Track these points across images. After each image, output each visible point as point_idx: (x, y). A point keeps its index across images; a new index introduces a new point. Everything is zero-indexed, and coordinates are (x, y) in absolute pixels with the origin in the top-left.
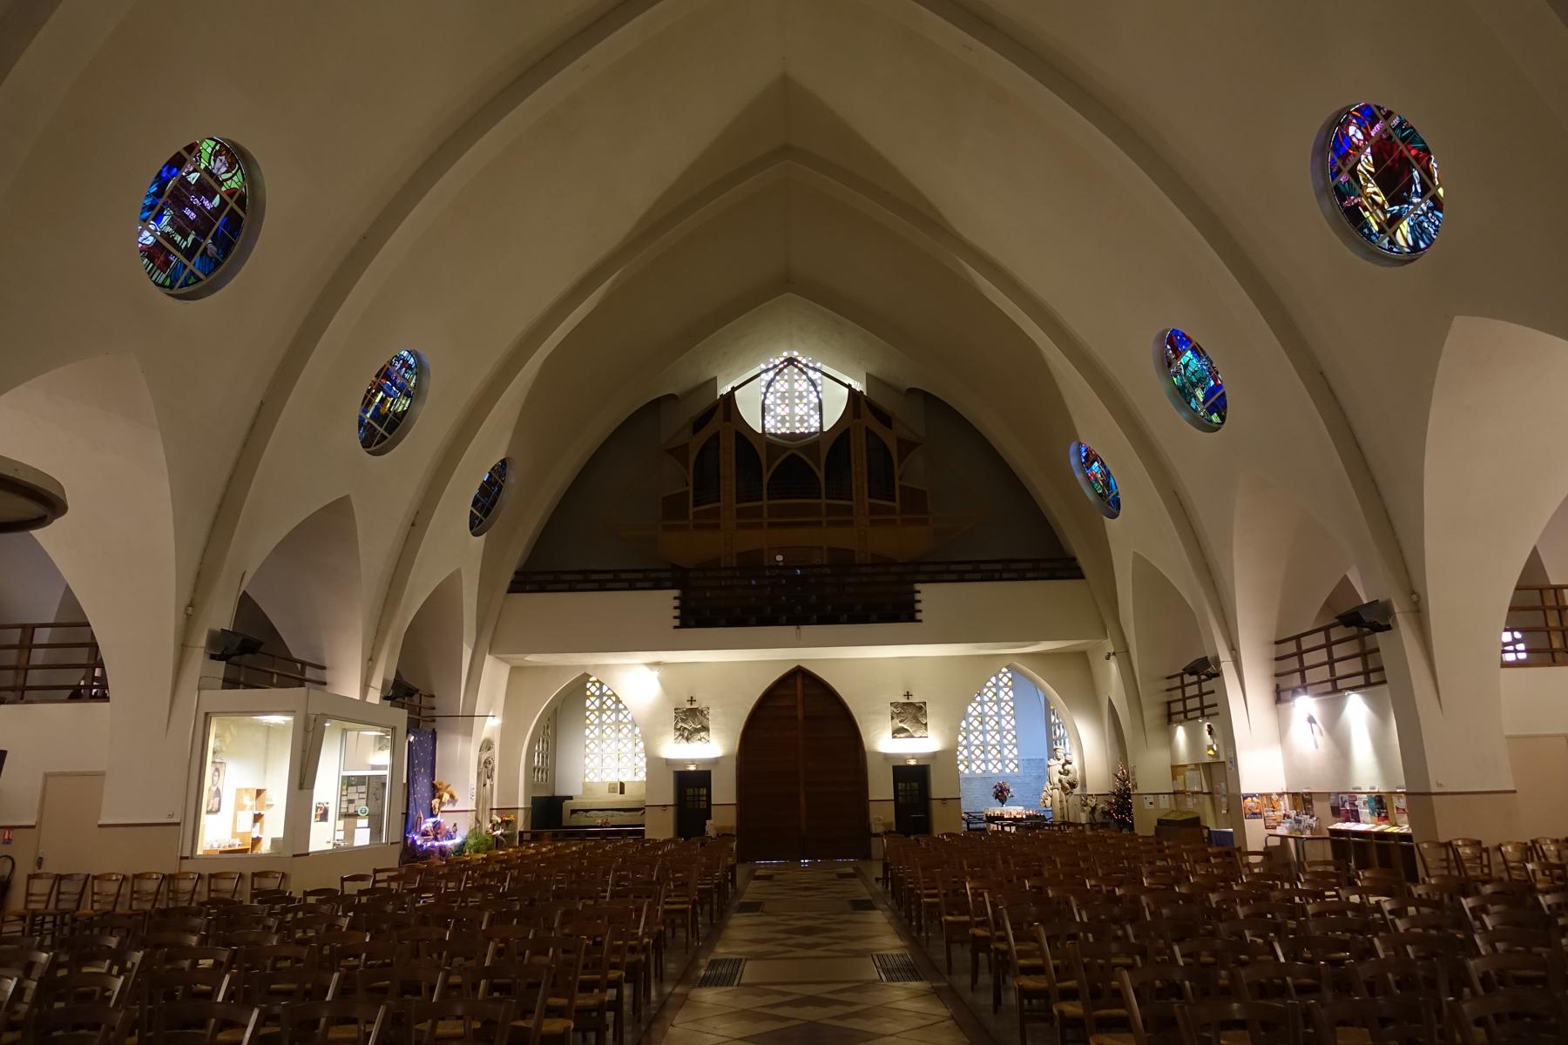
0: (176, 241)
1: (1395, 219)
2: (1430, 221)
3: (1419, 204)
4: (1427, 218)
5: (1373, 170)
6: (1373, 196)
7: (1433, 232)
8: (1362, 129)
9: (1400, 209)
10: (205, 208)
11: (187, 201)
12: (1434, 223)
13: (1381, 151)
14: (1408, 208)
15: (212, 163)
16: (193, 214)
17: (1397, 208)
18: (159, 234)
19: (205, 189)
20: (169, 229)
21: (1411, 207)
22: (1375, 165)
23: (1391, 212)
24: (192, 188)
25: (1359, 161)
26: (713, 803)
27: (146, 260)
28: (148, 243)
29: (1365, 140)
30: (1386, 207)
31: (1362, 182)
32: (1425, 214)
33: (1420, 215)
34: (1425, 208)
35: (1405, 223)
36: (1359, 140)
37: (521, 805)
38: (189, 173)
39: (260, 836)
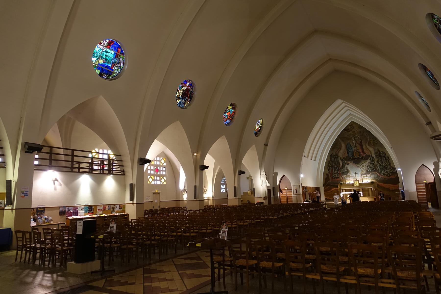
1: (180, 99)
3: (183, 101)
13: (187, 90)
22: (185, 90)
25: (185, 87)
26: (271, 197)
32: (182, 103)
35: (180, 100)
37: (301, 193)
39: (326, 174)
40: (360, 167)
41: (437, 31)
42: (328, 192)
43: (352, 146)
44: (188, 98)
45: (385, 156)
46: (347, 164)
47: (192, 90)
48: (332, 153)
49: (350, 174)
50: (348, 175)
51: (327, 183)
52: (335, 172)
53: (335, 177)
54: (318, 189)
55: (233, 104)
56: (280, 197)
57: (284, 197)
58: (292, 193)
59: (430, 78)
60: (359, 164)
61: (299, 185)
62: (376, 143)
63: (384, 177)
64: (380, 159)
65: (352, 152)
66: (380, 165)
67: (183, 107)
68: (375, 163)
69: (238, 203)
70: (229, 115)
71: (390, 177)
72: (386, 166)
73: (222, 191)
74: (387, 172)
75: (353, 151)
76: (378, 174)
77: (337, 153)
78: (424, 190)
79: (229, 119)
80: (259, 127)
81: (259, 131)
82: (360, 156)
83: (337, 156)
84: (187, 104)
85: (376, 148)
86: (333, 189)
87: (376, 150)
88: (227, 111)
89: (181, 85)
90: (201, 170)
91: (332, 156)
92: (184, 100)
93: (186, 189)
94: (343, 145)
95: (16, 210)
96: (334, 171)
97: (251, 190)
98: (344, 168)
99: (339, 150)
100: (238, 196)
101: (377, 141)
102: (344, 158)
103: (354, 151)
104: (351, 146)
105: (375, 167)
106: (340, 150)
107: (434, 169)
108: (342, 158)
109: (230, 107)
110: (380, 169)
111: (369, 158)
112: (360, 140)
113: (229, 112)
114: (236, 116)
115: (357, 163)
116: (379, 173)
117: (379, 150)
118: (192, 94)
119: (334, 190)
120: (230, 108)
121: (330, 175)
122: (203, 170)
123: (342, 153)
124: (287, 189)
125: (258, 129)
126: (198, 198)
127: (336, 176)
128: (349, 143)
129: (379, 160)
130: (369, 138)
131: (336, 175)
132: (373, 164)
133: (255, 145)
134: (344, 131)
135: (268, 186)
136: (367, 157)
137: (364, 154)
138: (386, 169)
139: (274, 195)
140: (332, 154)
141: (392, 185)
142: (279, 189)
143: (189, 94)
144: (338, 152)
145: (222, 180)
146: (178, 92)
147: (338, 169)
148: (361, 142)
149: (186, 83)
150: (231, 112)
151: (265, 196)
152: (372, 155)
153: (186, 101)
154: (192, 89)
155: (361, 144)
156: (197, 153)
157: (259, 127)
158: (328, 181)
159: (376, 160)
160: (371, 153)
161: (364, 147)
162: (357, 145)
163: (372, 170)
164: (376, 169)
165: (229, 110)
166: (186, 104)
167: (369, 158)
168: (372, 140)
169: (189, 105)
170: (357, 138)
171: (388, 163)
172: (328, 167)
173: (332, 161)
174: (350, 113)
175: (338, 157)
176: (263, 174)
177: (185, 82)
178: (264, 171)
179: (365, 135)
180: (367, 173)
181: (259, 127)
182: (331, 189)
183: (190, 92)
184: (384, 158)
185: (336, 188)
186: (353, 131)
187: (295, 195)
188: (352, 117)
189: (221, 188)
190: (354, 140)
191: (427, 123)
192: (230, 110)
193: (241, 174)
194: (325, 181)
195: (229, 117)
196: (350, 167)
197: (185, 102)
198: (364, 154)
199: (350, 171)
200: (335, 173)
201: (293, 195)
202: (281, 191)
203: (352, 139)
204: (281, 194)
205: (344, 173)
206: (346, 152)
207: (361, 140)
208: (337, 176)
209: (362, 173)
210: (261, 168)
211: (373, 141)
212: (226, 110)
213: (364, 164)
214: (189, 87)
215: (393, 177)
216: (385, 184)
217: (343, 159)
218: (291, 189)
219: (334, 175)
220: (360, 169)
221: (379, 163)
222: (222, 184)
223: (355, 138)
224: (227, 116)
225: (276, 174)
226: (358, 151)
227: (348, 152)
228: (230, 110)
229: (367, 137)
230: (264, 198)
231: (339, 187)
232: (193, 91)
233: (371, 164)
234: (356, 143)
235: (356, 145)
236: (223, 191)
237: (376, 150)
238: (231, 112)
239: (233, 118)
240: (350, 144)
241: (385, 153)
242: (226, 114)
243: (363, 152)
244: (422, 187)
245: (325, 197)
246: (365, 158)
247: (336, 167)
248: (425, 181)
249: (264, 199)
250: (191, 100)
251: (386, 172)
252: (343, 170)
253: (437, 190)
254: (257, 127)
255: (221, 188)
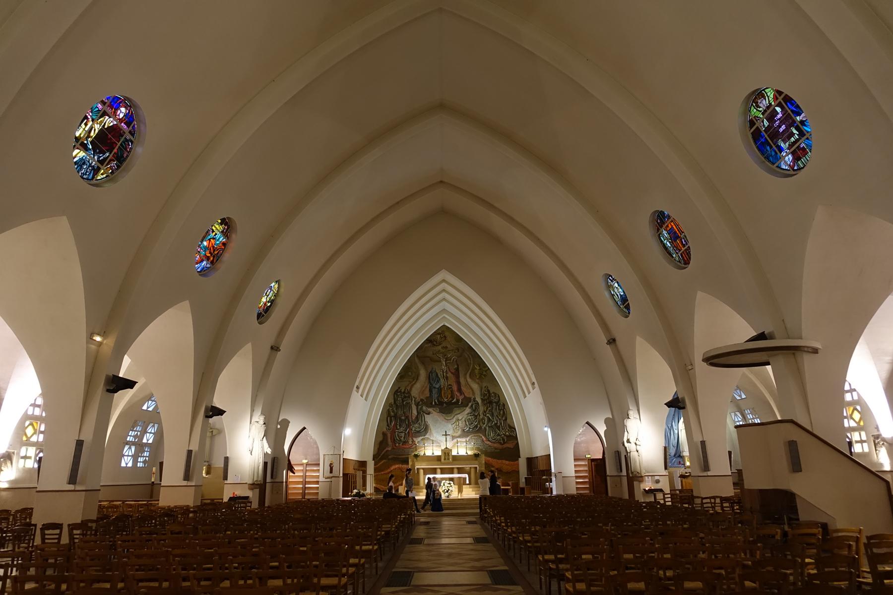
0: (794, 141)
1: (84, 147)
2: (87, 169)
3: (94, 160)
4: (89, 167)
5: (106, 127)
6: (93, 129)
7: (82, 172)
8: (124, 118)
9: (90, 149)
10: (781, 117)
11: (776, 129)
12: (87, 172)
14: (91, 154)
15: (761, 109)
16: (783, 127)
17: (91, 147)
18: (788, 151)
19: (771, 117)
20: (787, 144)
21: (92, 156)
22: (109, 127)
23: (88, 143)
24: (771, 124)
25: (110, 117)
26: (267, 481)
27: (799, 162)
28: (791, 158)
29: (119, 119)
30: (89, 139)
31: (99, 120)
33: (89, 162)
34: (93, 165)
35: (84, 154)
36: (119, 115)
37: (341, 475)
38: (764, 125)
39: (382, 432)
40: (452, 420)
41: (750, 136)
42: (383, 473)
43: (440, 377)
44: (113, 156)
45: (498, 403)
46: (426, 414)
47: (129, 137)
48: (399, 388)
49: (430, 435)
50: (427, 436)
51: (383, 453)
52: (401, 428)
53: (401, 440)
54: (362, 465)
55: (227, 222)
56: (286, 482)
57: (298, 483)
58: (321, 471)
59: (664, 246)
60: (450, 415)
61: (340, 455)
62: (484, 375)
63: (493, 444)
64: (490, 407)
65: (438, 388)
66: (489, 420)
67: (87, 179)
68: (480, 415)
69: (192, 502)
70: (210, 249)
71: (505, 446)
72: (499, 423)
73: (123, 464)
74: (500, 436)
75: (441, 386)
76: (483, 437)
77: (409, 388)
78: (586, 473)
79: (208, 258)
80: (268, 302)
81: (267, 310)
82: (453, 399)
83: (407, 395)
84: (104, 176)
85: (484, 384)
86: (393, 468)
87: (484, 389)
88: (209, 235)
89: (100, 106)
90: (108, 391)
91: (399, 394)
92: (99, 157)
93: (13, 453)
94: (423, 373)
95: (738, 429)
96: (398, 427)
97: (208, 462)
98: (420, 421)
99: (414, 382)
100: (194, 480)
101: (486, 371)
102: (422, 400)
103: (442, 387)
104: (438, 377)
105: (479, 422)
106: (415, 384)
107: (605, 432)
108: (418, 400)
109: (217, 226)
110: (487, 428)
111: (470, 404)
112: (456, 366)
113: (214, 239)
114: (227, 256)
115: (447, 414)
116: (485, 436)
117: (489, 389)
118: (126, 149)
119: (395, 469)
120: (219, 231)
121: (389, 435)
122: (115, 391)
123: (418, 390)
124: (307, 464)
125: (265, 304)
126: (81, 484)
127: (402, 439)
128: (434, 370)
129: (487, 408)
130: (472, 362)
131: (403, 436)
132: (476, 416)
133: (252, 345)
134: (427, 343)
135: (266, 455)
136: (466, 402)
137: (461, 395)
138: (498, 428)
139: (272, 477)
140: (398, 390)
141: (507, 462)
142: (288, 462)
143: (119, 144)
144: (410, 385)
145: (131, 432)
146: (86, 125)
147: (407, 423)
148: (457, 370)
149: (117, 108)
150: (218, 242)
151: (255, 480)
152: (475, 399)
153: (102, 165)
154: (130, 132)
155: (457, 374)
156: (103, 334)
157: (268, 302)
158: (384, 450)
159: (482, 409)
160: (474, 393)
161: (462, 380)
162: (449, 375)
163: (474, 429)
164: (481, 427)
165: (214, 233)
166: (102, 174)
167: (470, 404)
168: (478, 368)
169: (109, 179)
170: (450, 360)
171: (503, 417)
172: (387, 418)
173: (397, 405)
174: (443, 308)
175: (409, 398)
176: (257, 422)
177: (114, 103)
178: (262, 413)
179: (466, 355)
180: (464, 434)
181: (268, 299)
182: (389, 468)
183: (122, 139)
184: (496, 406)
185: (399, 464)
186: (444, 344)
187: (326, 478)
188: (447, 316)
189: (124, 455)
190: (445, 364)
191: (608, 341)
192: (216, 234)
193: (211, 417)
194: (379, 449)
195: (210, 253)
196: (433, 419)
197: (100, 165)
198: (461, 395)
199: (430, 429)
200: (401, 432)
201: (321, 479)
202: (291, 468)
203: (441, 362)
204: (291, 474)
205: (419, 432)
206: (426, 387)
207: (458, 366)
208: (404, 438)
209: (453, 435)
210: (254, 406)
211: (480, 369)
212: (207, 233)
213: (460, 417)
214: (122, 124)
215: (510, 445)
216: (495, 460)
217: (419, 402)
218: (319, 464)
219: (398, 435)
220: (450, 425)
221: (487, 415)
222: (127, 443)
223: (446, 361)
224: (206, 248)
225: (285, 424)
226: (450, 387)
227: (430, 387)
228: (216, 234)
229: (469, 361)
230: (253, 484)
231: (410, 463)
232: (132, 142)
233: (473, 417)
234: (448, 369)
235: (448, 375)
236: (127, 464)
237: (484, 389)
238: (218, 240)
239: (217, 260)
240: (435, 371)
241: (499, 396)
242: (205, 243)
243: (460, 390)
244: (584, 465)
245: (374, 485)
246: (462, 403)
247: (403, 418)
248: (589, 456)
249: (252, 486)
250: (119, 167)
251: (499, 435)
252: (417, 425)
253: (608, 473)
254: (264, 300)
255: (124, 455)
